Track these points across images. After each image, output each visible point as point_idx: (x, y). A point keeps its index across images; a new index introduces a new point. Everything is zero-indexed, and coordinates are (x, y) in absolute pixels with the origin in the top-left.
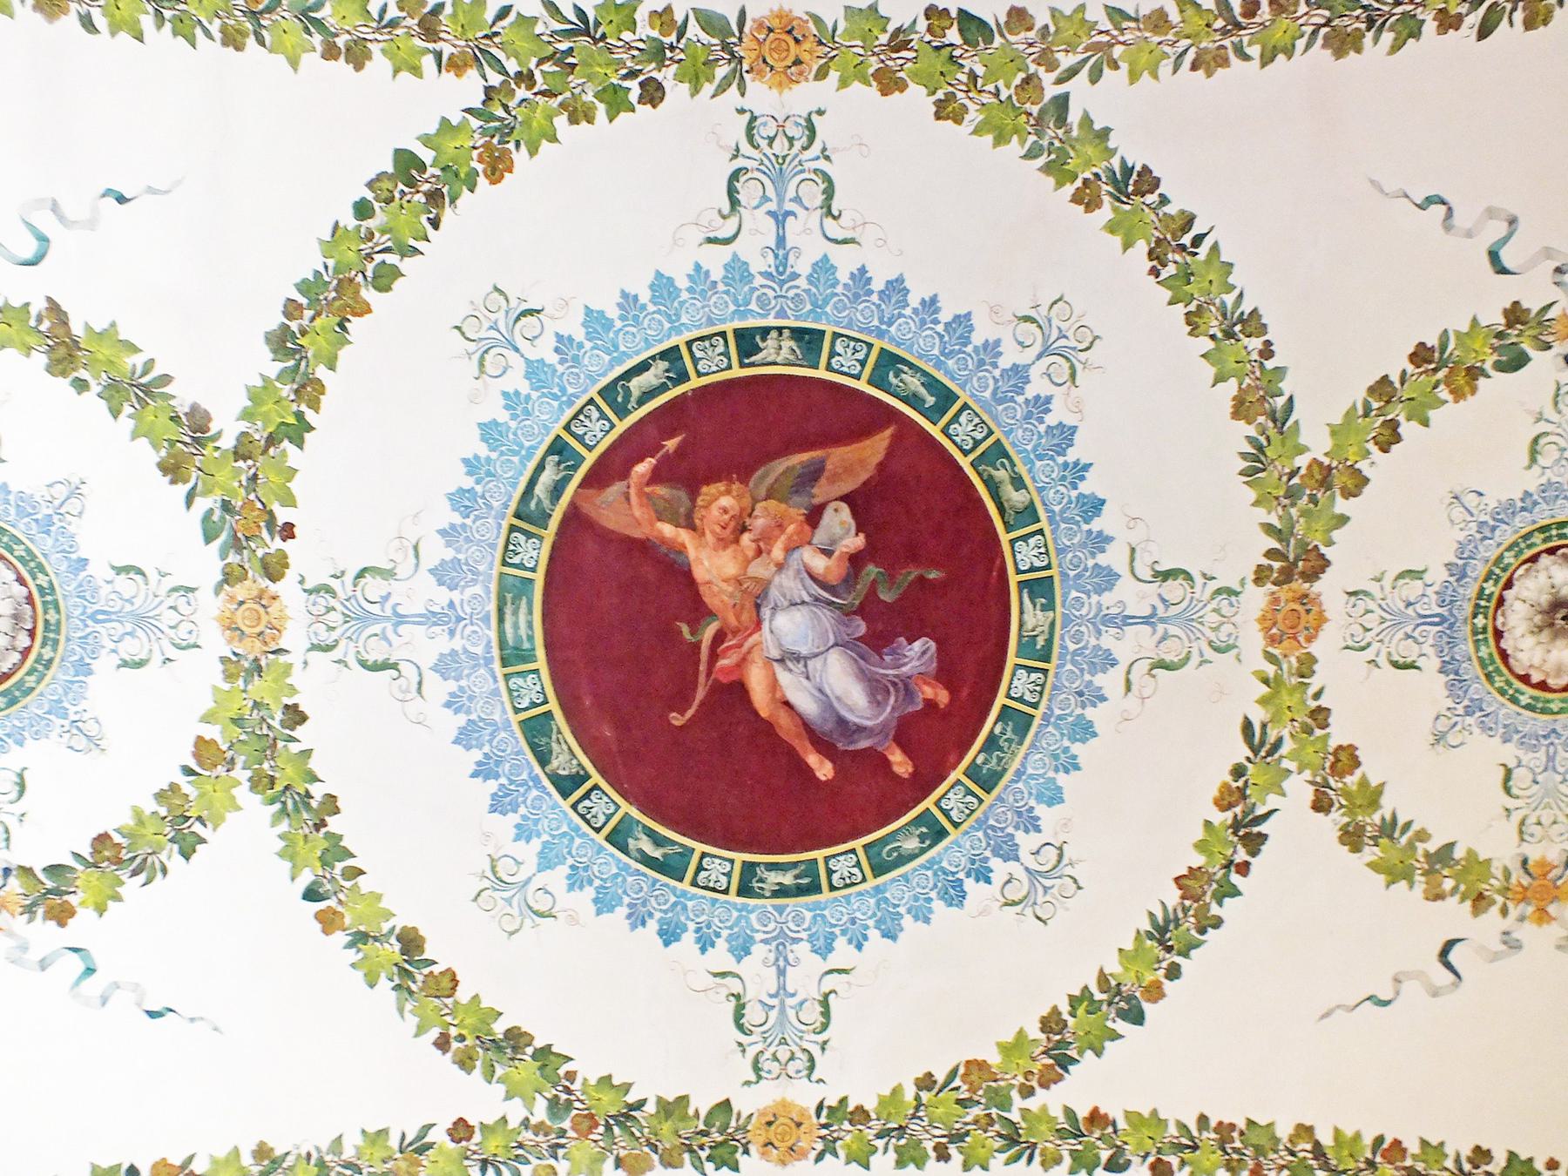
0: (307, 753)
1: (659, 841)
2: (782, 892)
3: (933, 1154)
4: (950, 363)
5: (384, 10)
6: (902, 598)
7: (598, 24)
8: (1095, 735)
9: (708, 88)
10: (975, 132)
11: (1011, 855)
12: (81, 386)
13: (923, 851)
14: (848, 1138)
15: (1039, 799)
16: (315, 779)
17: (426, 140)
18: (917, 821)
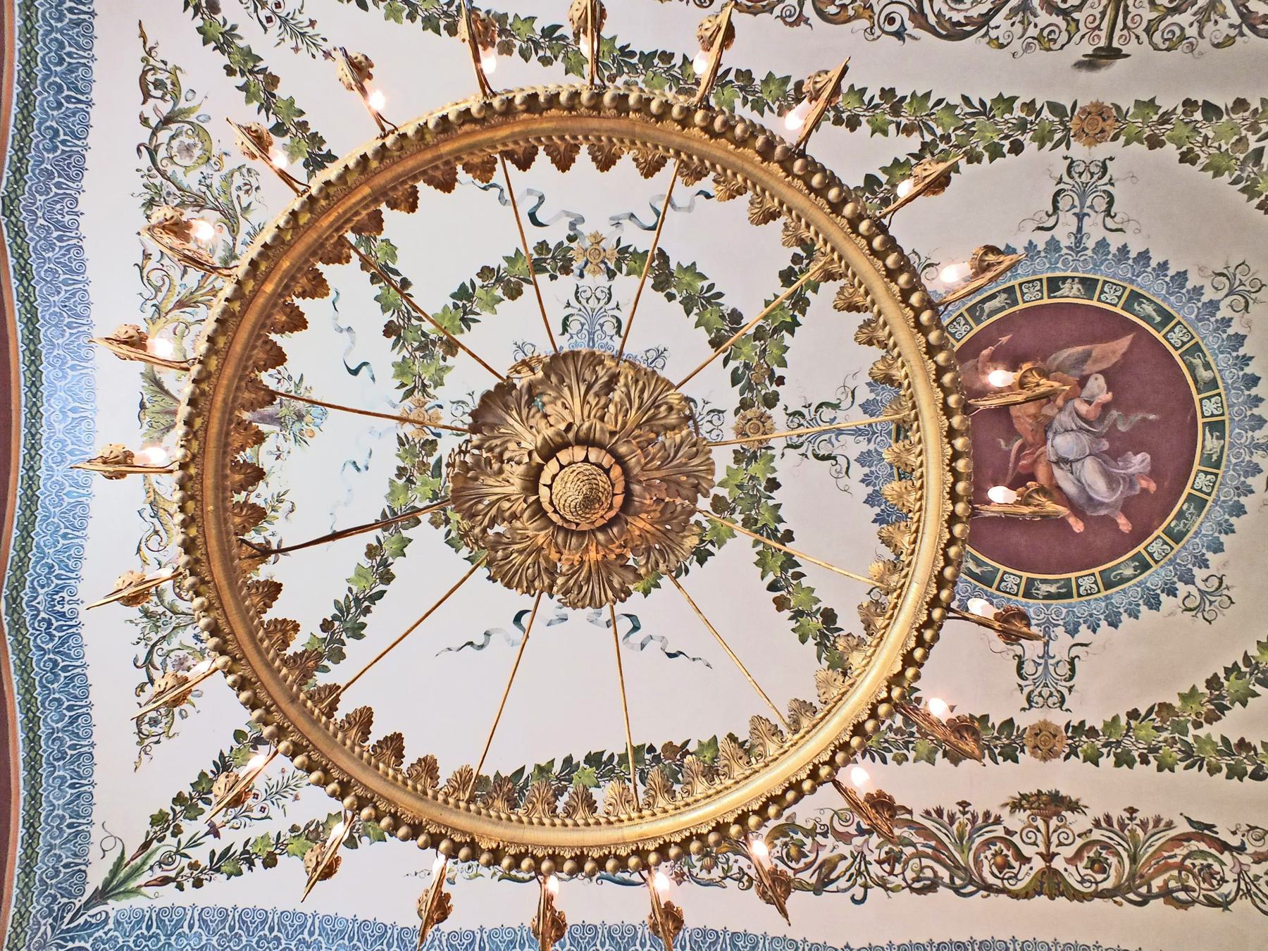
0: (778, 506)
1: (979, 563)
2: (1049, 596)
3: (1138, 760)
4: (1172, 298)
5: (872, 99)
6: (1132, 429)
7: (991, 109)
8: (1245, 513)
9: (1049, 145)
10: (1203, 170)
11: (1190, 580)
12: (671, 297)
13: (1136, 576)
14: (1085, 746)
15: (1208, 548)
16: (780, 520)
17: (884, 170)
18: (1133, 559)
